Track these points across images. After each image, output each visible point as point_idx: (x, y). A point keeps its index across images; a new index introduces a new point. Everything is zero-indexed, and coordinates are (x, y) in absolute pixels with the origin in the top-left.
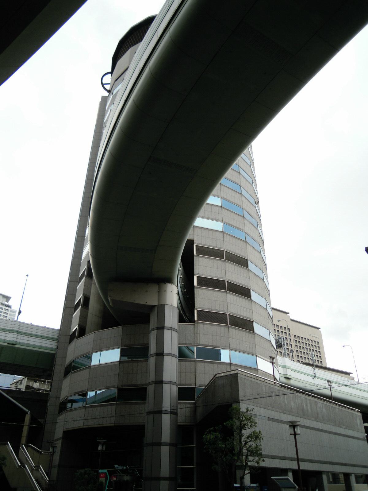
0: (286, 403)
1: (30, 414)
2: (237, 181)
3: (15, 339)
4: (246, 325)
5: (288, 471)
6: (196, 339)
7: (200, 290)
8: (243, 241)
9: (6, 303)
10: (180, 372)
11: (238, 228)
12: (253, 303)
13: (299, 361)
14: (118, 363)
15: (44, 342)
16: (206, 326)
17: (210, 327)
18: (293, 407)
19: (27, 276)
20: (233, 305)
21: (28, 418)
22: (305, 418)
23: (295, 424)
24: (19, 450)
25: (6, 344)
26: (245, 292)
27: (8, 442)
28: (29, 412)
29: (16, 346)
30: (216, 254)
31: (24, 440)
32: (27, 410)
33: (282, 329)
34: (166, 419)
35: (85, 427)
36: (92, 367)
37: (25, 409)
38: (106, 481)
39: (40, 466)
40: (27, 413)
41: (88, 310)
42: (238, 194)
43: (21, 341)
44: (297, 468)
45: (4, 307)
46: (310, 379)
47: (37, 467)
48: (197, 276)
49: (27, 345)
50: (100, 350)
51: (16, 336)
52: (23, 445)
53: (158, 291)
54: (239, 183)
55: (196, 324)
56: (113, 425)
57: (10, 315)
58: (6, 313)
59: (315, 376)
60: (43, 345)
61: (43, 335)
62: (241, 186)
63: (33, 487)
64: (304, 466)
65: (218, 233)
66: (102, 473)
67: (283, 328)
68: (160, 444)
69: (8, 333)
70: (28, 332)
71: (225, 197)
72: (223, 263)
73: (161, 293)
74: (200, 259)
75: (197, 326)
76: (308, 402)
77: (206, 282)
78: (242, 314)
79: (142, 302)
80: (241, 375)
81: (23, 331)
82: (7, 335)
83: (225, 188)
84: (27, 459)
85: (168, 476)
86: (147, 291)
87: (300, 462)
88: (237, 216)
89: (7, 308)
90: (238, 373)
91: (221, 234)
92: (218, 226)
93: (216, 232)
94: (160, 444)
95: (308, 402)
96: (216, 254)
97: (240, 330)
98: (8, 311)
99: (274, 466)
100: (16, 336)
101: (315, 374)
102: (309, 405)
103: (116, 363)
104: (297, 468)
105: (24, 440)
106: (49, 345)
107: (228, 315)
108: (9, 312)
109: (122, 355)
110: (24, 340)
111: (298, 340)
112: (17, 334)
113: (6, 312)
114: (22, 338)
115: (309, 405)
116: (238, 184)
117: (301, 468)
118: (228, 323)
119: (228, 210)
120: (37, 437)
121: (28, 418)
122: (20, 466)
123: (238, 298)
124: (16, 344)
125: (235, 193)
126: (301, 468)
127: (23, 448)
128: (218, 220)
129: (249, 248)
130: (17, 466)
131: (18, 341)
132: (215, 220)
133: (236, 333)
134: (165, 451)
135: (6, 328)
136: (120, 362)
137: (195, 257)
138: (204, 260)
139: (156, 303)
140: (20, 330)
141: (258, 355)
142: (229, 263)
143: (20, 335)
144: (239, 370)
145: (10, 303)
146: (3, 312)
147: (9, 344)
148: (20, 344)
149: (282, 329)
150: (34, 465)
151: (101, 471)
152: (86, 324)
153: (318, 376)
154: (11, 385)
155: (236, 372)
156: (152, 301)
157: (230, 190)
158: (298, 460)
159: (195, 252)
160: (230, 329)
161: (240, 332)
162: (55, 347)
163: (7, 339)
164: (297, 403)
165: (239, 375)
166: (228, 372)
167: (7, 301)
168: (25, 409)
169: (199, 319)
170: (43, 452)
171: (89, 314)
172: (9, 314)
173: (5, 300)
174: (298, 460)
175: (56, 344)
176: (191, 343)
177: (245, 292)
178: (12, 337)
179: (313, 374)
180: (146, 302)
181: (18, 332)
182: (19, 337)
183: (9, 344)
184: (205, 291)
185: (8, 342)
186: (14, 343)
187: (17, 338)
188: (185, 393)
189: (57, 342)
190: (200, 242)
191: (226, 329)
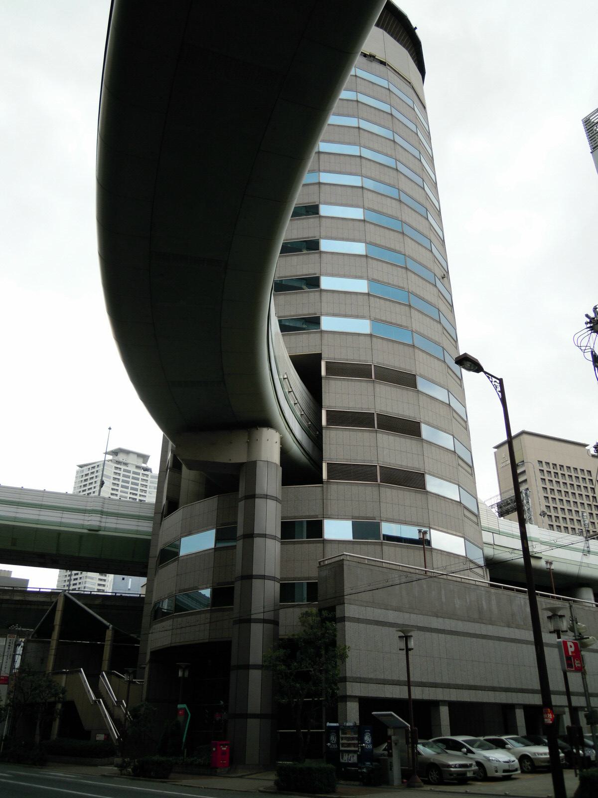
0: (444, 600)
1: (113, 628)
2: (398, 248)
3: (98, 523)
4: (413, 481)
5: (440, 704)
6: (324, 509)
7: (331, 431)
8: (408, 345)
9: (144, 465)
10: (285, 560)
11: (398, 325)
12: (425, 445)
13: (551, 526)
14: (213, 550)
15: (140, 524)
16: (341, 487)
17: (361, 488)
18: (457, 606)
19: (110, 429)
20: (390, 450)
21: (109, 634)
22: (484, 623)
23: (409, 635)
24: (99, 679)
25: (86, 531)
26: (410, 429)
27: (82, 669)
28: (111, 626)
29: (101, 533)
30: (359, 371)
31: (105, 665)
32: (108, 624)
33: (577, 474)
34: (257, 632)
35: (173, 645)
36: (180, 559)
37: (105, 622)
38: (186, 720)
39: (122, 701)
40: (108, 627)
41: (181, 474)
42: (399, 269)
43: (108, 525)
44: (407, 697)
45: (142, 472)
46: (578, 557)
47: (119, 702)
48: (327, 411)
49: (116, 530)
50: (190, 534)
51: (98, 519)
52: (104, 673)
53: (248, 442)
54: (402, 250)
55: (325, 486)
56: (207, 641)
57: (151, 483)
58: (145, 480)
59: (589, 552)
60: (140, 528)
61: (138, 513)
62: (405, 255)
63: (108, 729)
64: (418, 694)
65: (362, 338)
66: (181, 709)
67: (579, 470)
68: (247, 667)
69: (88, 515)
70: (116, 511)
71: (375, 277)
72: (371, 385)
73: (251, 444)
74: (332, 382)
75: (327, 488)
76: (493, 597)
77: (340, 418)
78: (404, 464)
79: (226, 460)
80: (351, 562)
81: (109, 510)
82: (86, 518)
83: (375, 262)
84: (107, 691)
85: (258, 712)
86: (231, 443)
87: (412, 688)
88: (397, 305)
89: (146, 473)
90: (343, 560)
91: (368, 339)
92: (363, 326)
93: (359, 336)
94: (247, 667)
95: (493, 597)
96: (359, 371)
97: (404, 490)
98: (148, 477)
99: (485, 700)
100: (98, 519)
101: (588, 547)
102: (494, 603)
103: (211, 551)
104: (407, 697)
105: (105, 665)
106: (146, 527)
107: (378, 468)
108: (149, 479)
109: (218, 539)
110: (111, 523)
111: (550, 496)
112: (99, 515)
113: (145, 478)
114: (108, 520)
115: (494, 603)
116: (399, 252)
117: (413, 697)
118: (379, 480)
119: (380, 298)
120: (126, 658)
121: (109, 634)
122: (95, 701)
123: (397, 439)
124: (100, 531)
125: (394, 268)
126: (413, 697)
127: (103, 676)
128: (363, 317)
129: (420, 355)
130: (91, 701)
131: (103, 525)
132: (357, 317)
133: (392, 495)
134: (255, 676)
135: (84, 508)
136: (216, 549)
137: (323, 381)
138: (339, 383)
139: (244, 460)
140: (104, 510)
141: (433, 526)
142: (380, 383)
143: (105, 516)
144: (347, 555)
145: (149, 465)
146: (140, 479)
147: (89, 530)
148: (105, 529)
149: (577, 474)
150: (116, 700)
151: (180, 706)
152: (179, 495)
153: (593, 550)
154: (142, 587)
155: (342, 558)
156: (236, 455)
157: (385, 265)
158: (409, 684)
159: (323, 373)
160: (382, 489)
161: (401, 493)
162: (150, 530)
163: (86, 523)
164: (468, 601)
165: (345, 562)
166: (337, 556)
167: (145, 462)
168: (105, 622)
169: (329, 477)
170: (138, 681)
171: (183, 480)
172: (149, 482)
173: (141, 460)
174: (409, 684)
175: (151, 525)
176: (317, 514)
177: (410, 428)
178: (93, 521)
179: (586, 549)
180: (230, 460)
181: (102, 513)
182: (104, 520)
183: (89, 530)
184: (340, 433)
185: (89, 528)
186: (97, 529)
187: (100, 521)
188: (288, 591)
189: (152, 522)
190: (332, 356)
191: (375, 489)
